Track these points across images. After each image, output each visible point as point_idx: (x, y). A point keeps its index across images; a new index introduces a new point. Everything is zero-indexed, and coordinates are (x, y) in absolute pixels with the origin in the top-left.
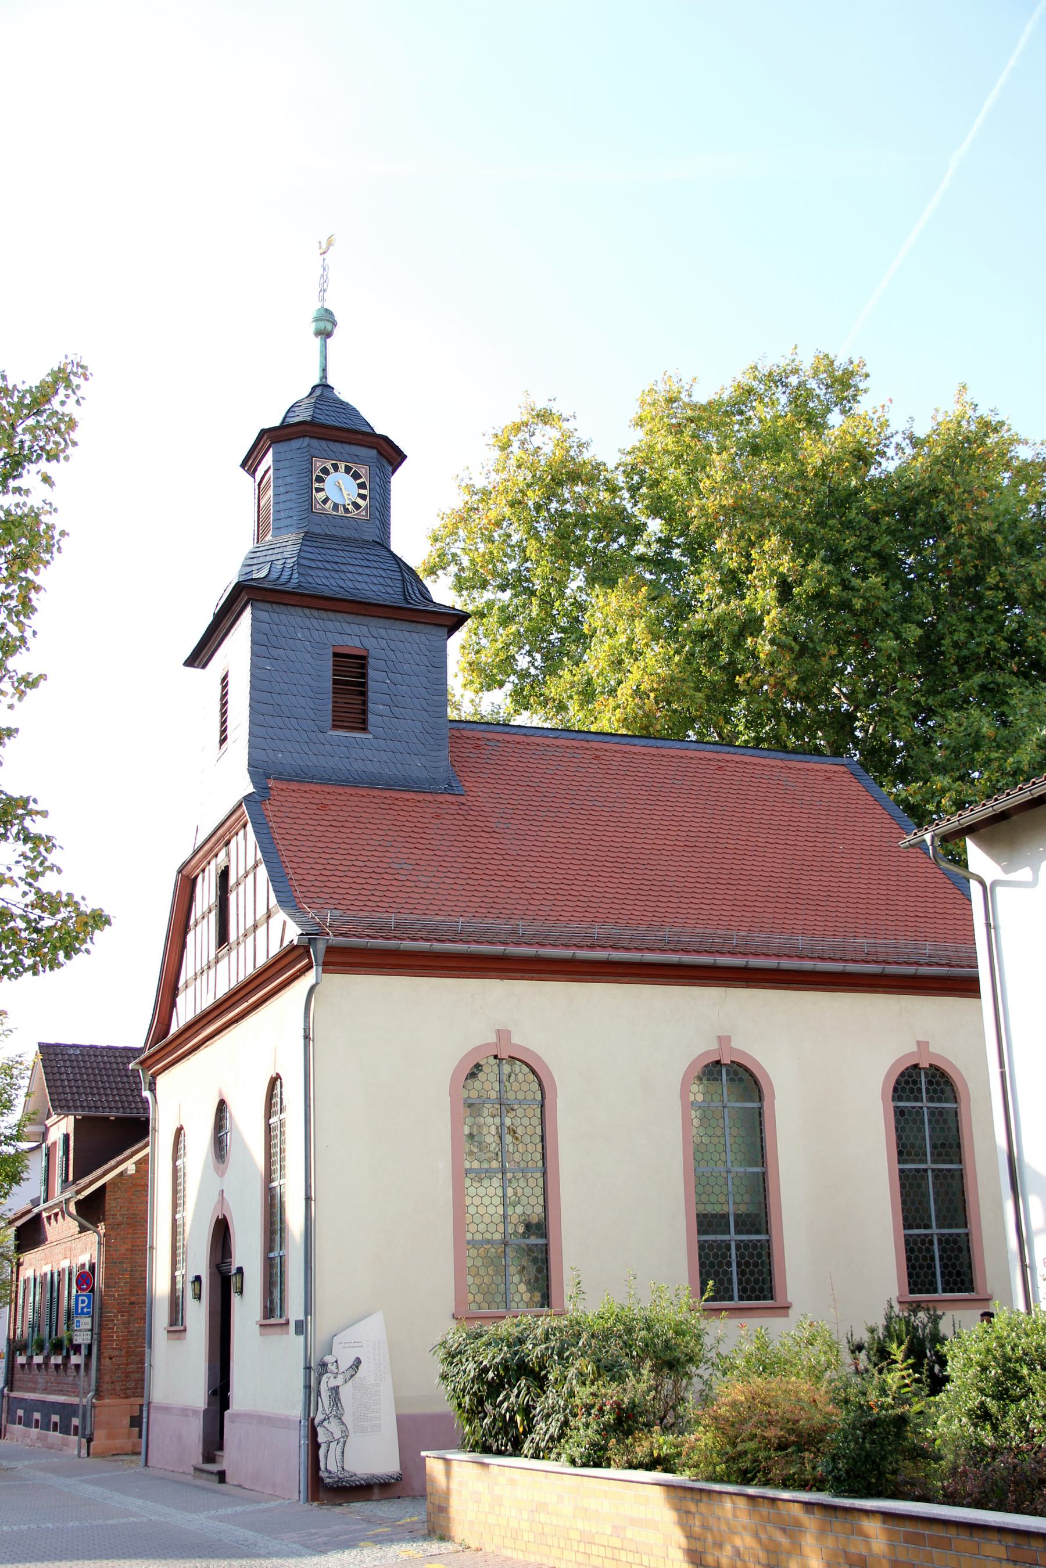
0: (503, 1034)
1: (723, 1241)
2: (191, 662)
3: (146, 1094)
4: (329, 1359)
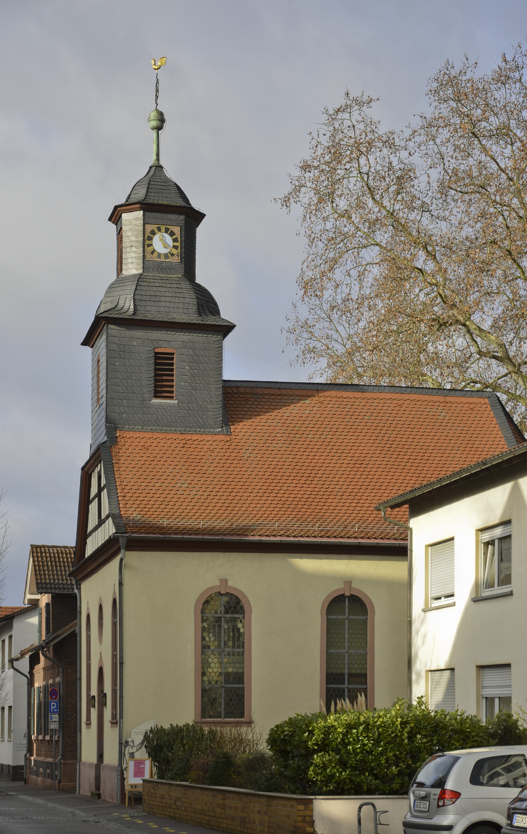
0: (224, 581)
1: (341, 688)
2: (85, 343)
3: (76, 591)
4: (129, 740)
